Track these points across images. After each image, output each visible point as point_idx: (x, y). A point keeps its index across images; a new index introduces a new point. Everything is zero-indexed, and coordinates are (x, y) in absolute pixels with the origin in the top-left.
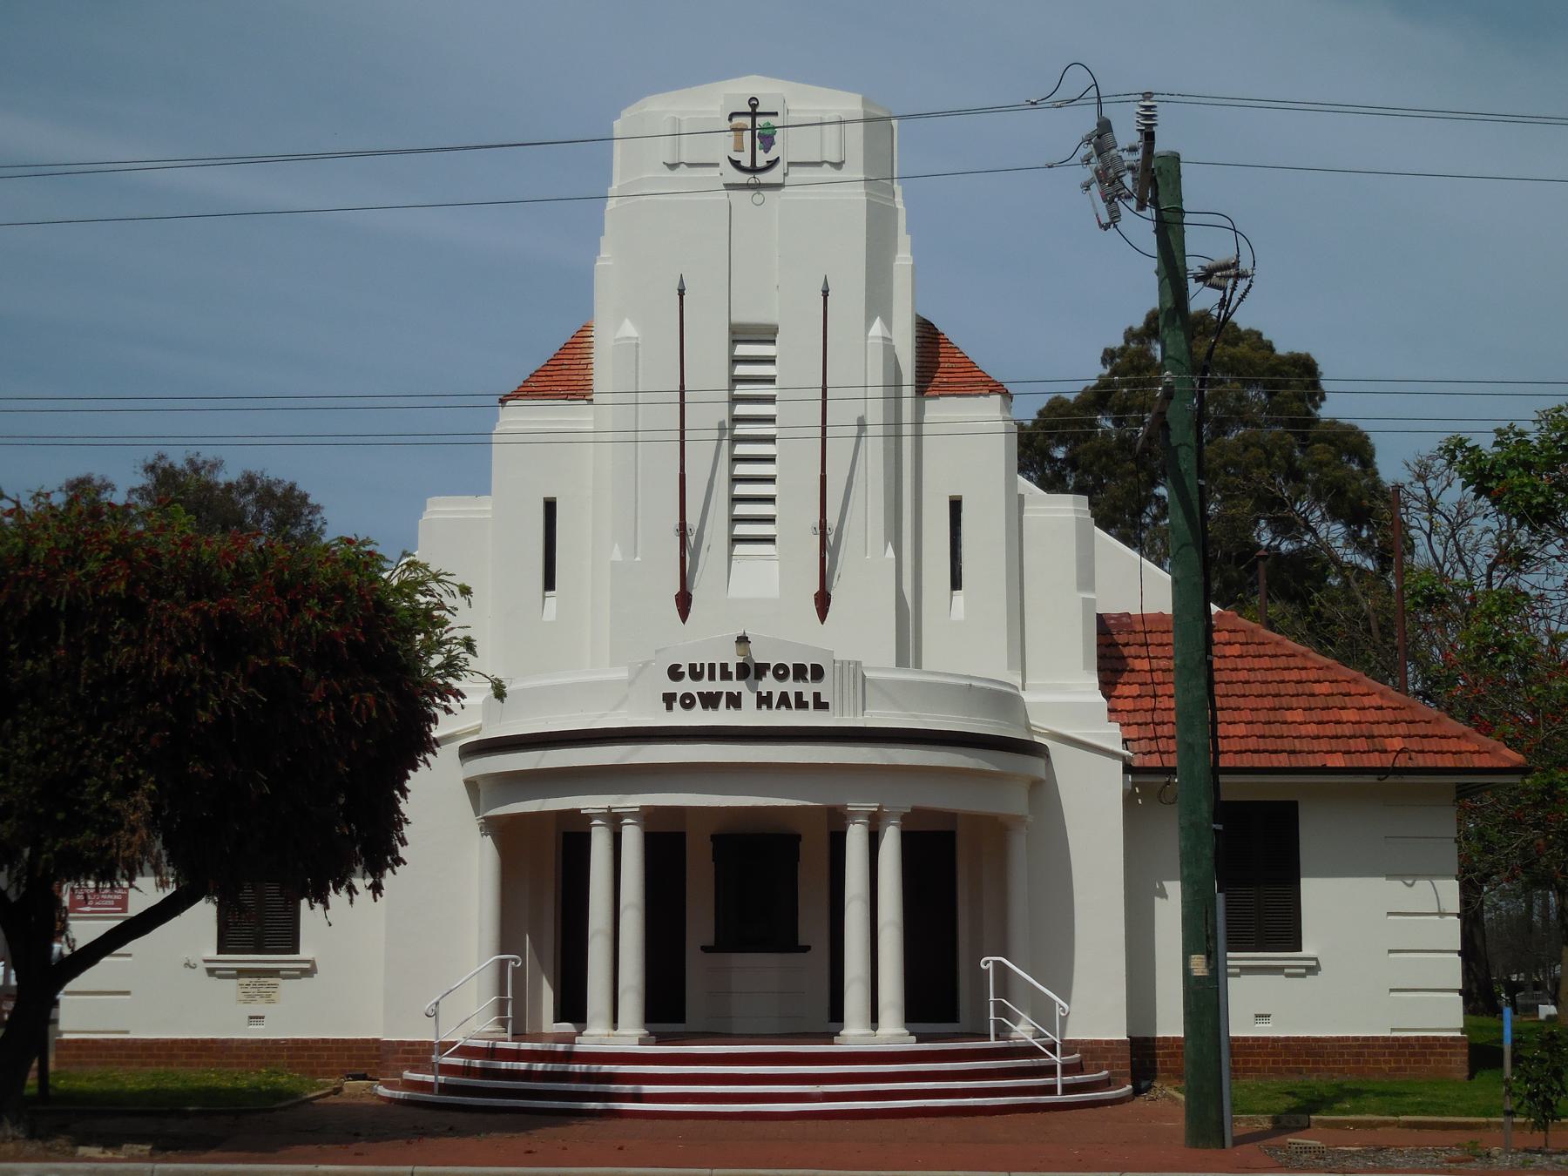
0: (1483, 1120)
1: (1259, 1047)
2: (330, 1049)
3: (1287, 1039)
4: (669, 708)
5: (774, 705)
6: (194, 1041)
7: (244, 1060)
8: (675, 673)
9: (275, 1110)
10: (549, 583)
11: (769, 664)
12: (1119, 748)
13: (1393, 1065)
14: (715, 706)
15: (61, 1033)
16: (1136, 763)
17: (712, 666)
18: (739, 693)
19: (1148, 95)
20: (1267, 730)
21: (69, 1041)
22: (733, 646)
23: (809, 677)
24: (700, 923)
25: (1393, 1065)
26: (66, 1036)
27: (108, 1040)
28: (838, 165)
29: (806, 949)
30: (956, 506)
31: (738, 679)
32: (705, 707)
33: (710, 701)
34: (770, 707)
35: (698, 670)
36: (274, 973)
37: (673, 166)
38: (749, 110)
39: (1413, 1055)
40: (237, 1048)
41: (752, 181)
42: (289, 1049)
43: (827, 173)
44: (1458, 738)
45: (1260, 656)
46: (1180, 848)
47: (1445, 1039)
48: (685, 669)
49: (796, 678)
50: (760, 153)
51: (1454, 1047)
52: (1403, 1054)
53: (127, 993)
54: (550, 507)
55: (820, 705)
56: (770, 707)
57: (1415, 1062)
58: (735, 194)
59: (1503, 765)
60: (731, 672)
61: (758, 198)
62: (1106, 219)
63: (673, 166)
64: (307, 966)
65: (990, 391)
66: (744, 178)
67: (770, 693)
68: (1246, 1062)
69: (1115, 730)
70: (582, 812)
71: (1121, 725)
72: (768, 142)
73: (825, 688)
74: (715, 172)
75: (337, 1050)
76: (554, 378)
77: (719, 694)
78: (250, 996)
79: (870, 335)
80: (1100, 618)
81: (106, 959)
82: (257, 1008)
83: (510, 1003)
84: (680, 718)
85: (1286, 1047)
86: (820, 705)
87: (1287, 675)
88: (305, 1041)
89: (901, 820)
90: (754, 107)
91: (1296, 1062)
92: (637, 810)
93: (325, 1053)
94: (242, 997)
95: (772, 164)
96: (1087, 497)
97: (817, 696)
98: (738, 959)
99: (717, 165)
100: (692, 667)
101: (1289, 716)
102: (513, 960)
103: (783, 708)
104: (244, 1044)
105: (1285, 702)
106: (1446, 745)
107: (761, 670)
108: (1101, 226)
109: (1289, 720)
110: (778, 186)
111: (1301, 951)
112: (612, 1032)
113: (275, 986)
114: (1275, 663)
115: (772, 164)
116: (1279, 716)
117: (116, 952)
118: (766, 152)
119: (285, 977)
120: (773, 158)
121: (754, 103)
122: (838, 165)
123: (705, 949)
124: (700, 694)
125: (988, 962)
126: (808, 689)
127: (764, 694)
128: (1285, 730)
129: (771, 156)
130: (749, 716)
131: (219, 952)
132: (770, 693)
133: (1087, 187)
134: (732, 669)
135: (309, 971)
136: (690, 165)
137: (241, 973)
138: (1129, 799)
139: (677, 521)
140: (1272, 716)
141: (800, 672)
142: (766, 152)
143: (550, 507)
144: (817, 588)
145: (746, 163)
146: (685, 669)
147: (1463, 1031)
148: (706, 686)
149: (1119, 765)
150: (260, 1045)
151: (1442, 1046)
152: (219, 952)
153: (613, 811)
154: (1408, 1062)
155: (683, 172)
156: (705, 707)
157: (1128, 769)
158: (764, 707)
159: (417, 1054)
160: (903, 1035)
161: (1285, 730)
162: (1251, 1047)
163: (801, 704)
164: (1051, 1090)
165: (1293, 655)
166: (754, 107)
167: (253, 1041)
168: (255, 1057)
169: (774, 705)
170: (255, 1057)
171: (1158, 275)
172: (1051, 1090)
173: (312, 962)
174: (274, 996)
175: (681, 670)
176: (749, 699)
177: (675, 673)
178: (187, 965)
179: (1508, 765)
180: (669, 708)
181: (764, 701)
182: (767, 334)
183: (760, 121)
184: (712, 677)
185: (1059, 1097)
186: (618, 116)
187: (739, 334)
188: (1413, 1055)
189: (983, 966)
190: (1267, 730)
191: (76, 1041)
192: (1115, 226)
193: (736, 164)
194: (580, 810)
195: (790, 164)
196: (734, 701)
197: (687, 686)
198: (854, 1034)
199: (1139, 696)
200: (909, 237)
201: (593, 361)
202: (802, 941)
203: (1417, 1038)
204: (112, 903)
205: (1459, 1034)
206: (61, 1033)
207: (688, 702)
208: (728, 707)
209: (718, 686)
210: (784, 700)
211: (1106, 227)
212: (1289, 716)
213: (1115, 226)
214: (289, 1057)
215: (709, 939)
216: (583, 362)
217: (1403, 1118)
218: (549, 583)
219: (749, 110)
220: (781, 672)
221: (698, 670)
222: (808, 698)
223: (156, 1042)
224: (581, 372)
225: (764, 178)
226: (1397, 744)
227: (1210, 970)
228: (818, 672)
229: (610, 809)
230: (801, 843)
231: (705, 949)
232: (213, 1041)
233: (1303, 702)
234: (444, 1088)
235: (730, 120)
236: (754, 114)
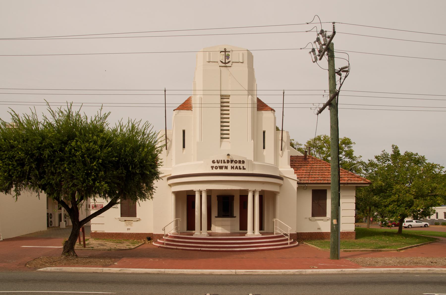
1: (318, 234)
2: (143, 235)
4: (212, 169)
8: (213, 162)
10: (184, 147)
12: (296, 179)
13: (342, 237)
16: (299, 182)
17: (221, 161)
18: (227, 166)
19: (334, 23)
22: (226, 156)
23: (242, 163)
24: (215, 213)
25: (342, 237)
26: (92, 232)
28: (242, 63)
30: (264, 132)
31: (227, 163)
33: (221, 168)
34: (234, 169)
35: (219, 161)
37: (209, 62)
38: (224, 51)
39: (345, 235)
42: (135, 235)
43: (240, 64)
46: (331, 197)
47: (351, 232)
48: (216, 161)
49: (239, 163)
51: (352, 233)
52: (344, 235)
54: (184, 132)
57: (346, 236)
58: (221, 68)
60: (225, 162)
62: (314, 60)
64: (138, 219)
66: (223, 65)
67: (234, 166)
71: (297, 175)
75: (144, 235)
77: (223, 166)
79: (249, 97)
83: (179, 228)
84: (215, 171)
89: (259, 192)
94: (126, 225)
95: (229, 62)
97: (243, 167)
100: (217, 161)
103: (236, 169)
104: (126, 234)
105: (324, 171)
107: (232, 161)
108: (313, 62)
109: (312, 177)
111: (136, 217)
113: (132, 223)
115: (229, 62)
120: (229, 61)
121: (225, 49)
122: (242, 63)
124: (219, 166)
125: (274, 220)
126: (241, 165)
129: (229, 60)
130: (229, 171)
131: (121, 217)
132: (234, 166)
133: (310, 53)
134: (226, 161)
135: (139, 220)
140: (322, 174)
141: (240, 162)
143: (184, 132)
145: (224, 62)
146: (216, 161)
147: (354, 231)
148: (220, 164)
149: (296, 182)
151: (351, 233)
153: (200, 190)
154: (345, 236)
155: (211, 63)
156: (220, 169)
157: (298, 183)
158: (233, 169)
163: (240, 169)
164: (287, 244)
165: (324, 163)
167: (128, 233)
168: (129, 236)
170: (129, 236)
171: (328, 71)
172: (287, 244)
173: (139, 219)
174: (132, 225)
175: (215, 161)
176: (229, 168)
177: (213, 162)
180: (212, 169)
181: (232, 168)
183: (227, 53)
184: (221, 163)
185: (289, 245)
188: (345, 235)
189: (273, 220)
192: (316, 62)
193: (222, 62)
196: (226, 168)
197: (216, 164)
198: (249, 233)
201: (192, 100)
202: (234, 216)
203: (346, 232)
204: (100, 207)
205: (354, 231)
207: (216, 168)
208: (225, 169)
209: (223, 164)
210: (237, 167)
211: (314, 62)
212: (326, 174)
213: (316, 62)
214: (135, 236)
215: (217, 215)
218: (184, 147)
219: (224, 51)
220: (236, 162)
221: (219, 161)
222: (242, 167)
224: (190, 105)
225: (227, 65)
226: (347, 179)
227: (337, 223)
228: (243, 162)
231: (216, 217)
232: (121, 233)
233: (327, 171)
234: (167, 244)
235: (220, 53)
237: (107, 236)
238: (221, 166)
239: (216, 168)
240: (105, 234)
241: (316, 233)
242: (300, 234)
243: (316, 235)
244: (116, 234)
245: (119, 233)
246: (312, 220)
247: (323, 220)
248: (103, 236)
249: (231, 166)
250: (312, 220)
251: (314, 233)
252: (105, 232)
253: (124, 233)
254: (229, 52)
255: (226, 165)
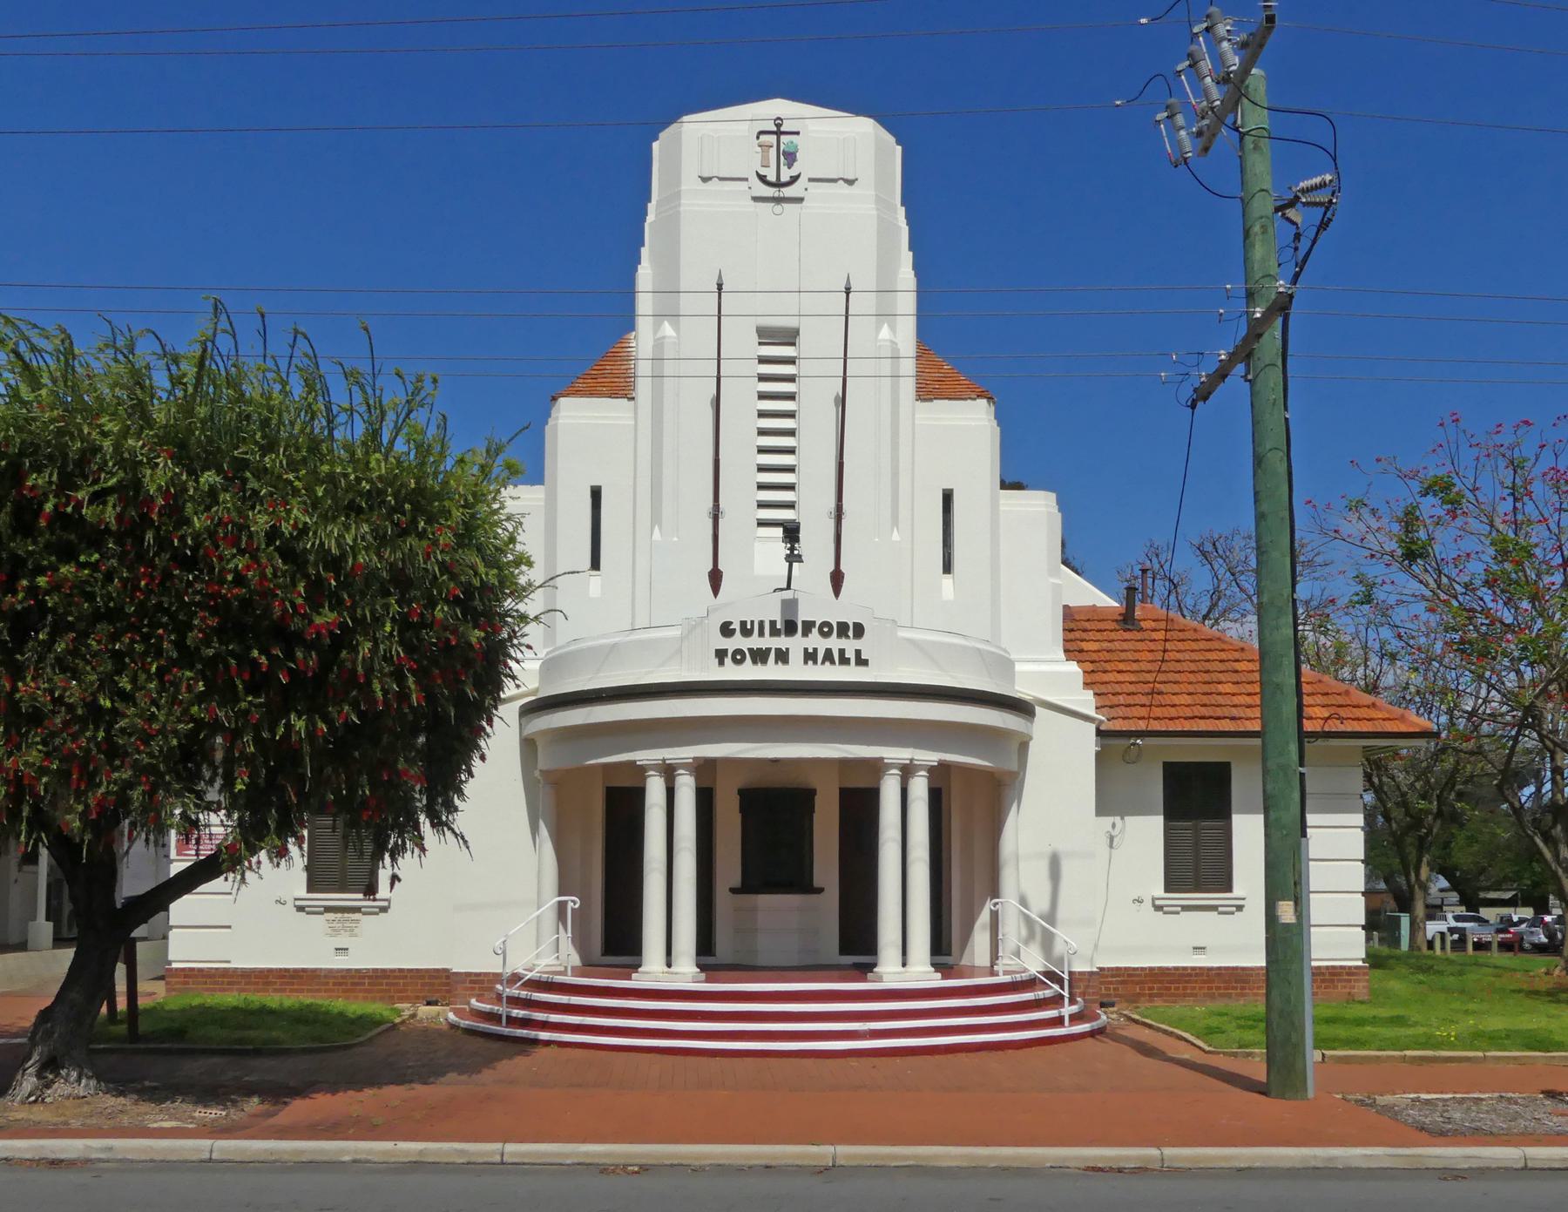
0: (1480, 1054)
1: (1196, 975)
3: (1219, 968)
4: (721, 663)
5: (820, 660)
6: (287, 970)
7: (331, 987)
8: (726, 630)
9: (355, 1045)
11: (814, 622)
14: (764, 661)
15: (170, 963)
20: (1205, 700)
21: (177, 969)
23: (851, 633)
26: (175, 965)
27: (212, 968)
28: (850, 182)
29: (820, 890)
32: (754, 662)
33: (760, 656)
34: (815, 662)
35: (749, 627)
36: (357, 910)
37: (705, 180)
38: (775, 129)
40: (326, 977)
41: (776, 195)
42: (370, 977)
44: (1368, 707)
45: (1183, 640)
47: (1350, 967)
49: (840, 635)
50: (784, 169)
53: (229, 927)
55: (862, 662)
56: (815, 662)
59: (1411, 730)
61: (778, 208)
63: (705, 180)
65: (978, 396)
66: (770, 192)
67: (815, 650)
68: (1185, 988)
69: (1089, 695)
70: (638, 763)
72: (791, 157)
73: (864, 645)
74: (743, 186)
76: (599, 380)
77: (769, 650)
78: (335, 930)
80: (1066, 607)
81: (185, 897)
82: (342, 941)
85: (1219, 975)
86: (862, 662)
87: (1210, 656)
88: (383, 970)
90: (778, 126)
91: (1226, 989)
92: (691, 761)
93: (401, 981)
94: (329, 931)
95: (794, 179)
96: (1050, 498)
97: (858, 653)
98: (765, 900)
99: (746, 180)
100: (743, 624)
101: (1221, 688)
102: (572, 901)
103: (827, 664)
104: (330, 973)
105: (1215, 677)
106: (1358, 713)
110: (800, 200)
111: (1229, 889)
112: (666, 969)
114: (1194, 646)
115: (794, 179)
116: (1212, 688)
117: (199, 889)
118: (789, 168)
119: (365, 914)
123: (733, 891)
126: (850, 646)
127: (811, 650)
128: (1220, 700)
129: (794, 172)
130: (796, 671)
132: (815, 650)
136: (721, 179)
137: (328, 909)
138: (1100, 758)
139: (710, 504)
141: (843, 629)
142: (789, 168)
144: (832, 568)
145: (772, 178)
146: (736, 626)
148: (755, 642)
150: (344, 974)
151: (1348, 974)
152: (309, 891)
153: (667, 762)
157: (1100, 733)
158: (810, 662)
159: (481, 983)
160: (929, 972)
161: (1220, 700)
162: (1190, 975)
163: (844, 661)
164: (1058, 1021)
166: (778, 126)
169: (820, 660)
170: (340, 984)
172: (1058, 1021)
173: (388, 900)
174: (356, 930)
176: (796, 656)
177: (726, 630)
178: (278, 902)
179: (1418, 730)
180: (721, 663)
181: (810, 656)
182: (789, 337)
183: (784, 138)
184: (761, 634)
186: (656, 139)
187: (768, 335)
190: (1205, 700)
191: (183, 969)
193: (762, 178)
194: (635, 761)
195: (811, 180)
196: (782, 656)
197: (738, 642)
199: (1093, 671)
200: (911, 253)
202: (817, 883)
203: (1327, 967)
205: (1360, 963)
206: (170, 963)
207: (739, 657)
208: (776, 662)
210: (828, 656)
212: (1221, 688)
215: (736, 880)
216: (623, 367)
217: (1408, 1053)
219: (775, 129)
220: (825, 630)
221: (749, 627)
222: (850, 654)
223: (253, 971)
225: (788, 192)
228: (859, 630)
229: (664, 760)
230: (816, 797)
231: (733, 891)
232: (304, 970)
235: (758, 138)
236: (779, 133)
237: (239, 983)
238: (759, 650)
239: (738, 656)
240: (232, 976)
241: (1185, 968)
242: (1113, 976)
243: (1187, 982)
244: (284, 977)
245: (296, 970)
246: (1220, 909)
247: (1214, 908)
248: (223, 983)
249: (806, 650)
250: (1165, 909)
251: (1176, 969)
252: (236, 964)
253: (321, 969)
254: (795, 136)
255: (782, 642)
